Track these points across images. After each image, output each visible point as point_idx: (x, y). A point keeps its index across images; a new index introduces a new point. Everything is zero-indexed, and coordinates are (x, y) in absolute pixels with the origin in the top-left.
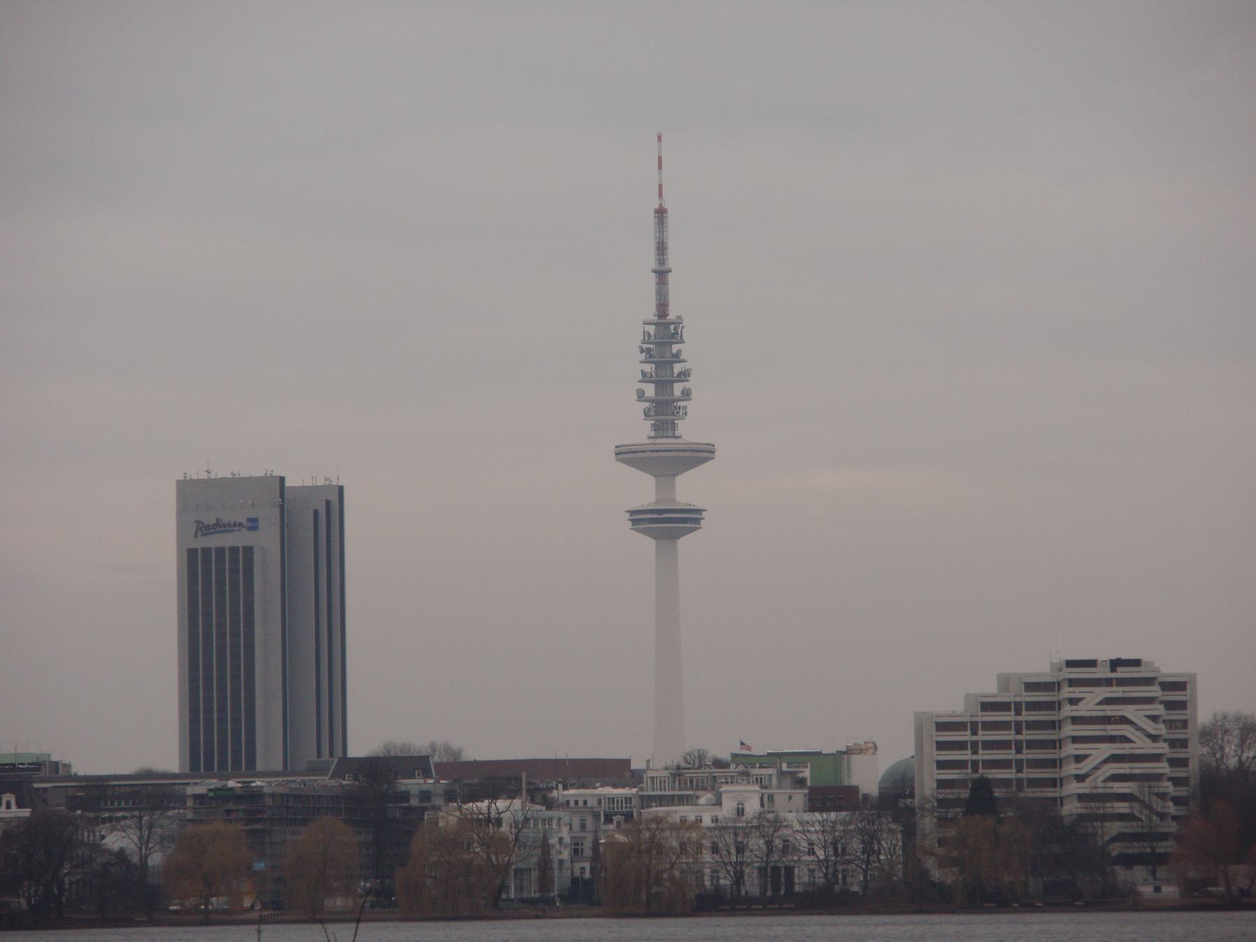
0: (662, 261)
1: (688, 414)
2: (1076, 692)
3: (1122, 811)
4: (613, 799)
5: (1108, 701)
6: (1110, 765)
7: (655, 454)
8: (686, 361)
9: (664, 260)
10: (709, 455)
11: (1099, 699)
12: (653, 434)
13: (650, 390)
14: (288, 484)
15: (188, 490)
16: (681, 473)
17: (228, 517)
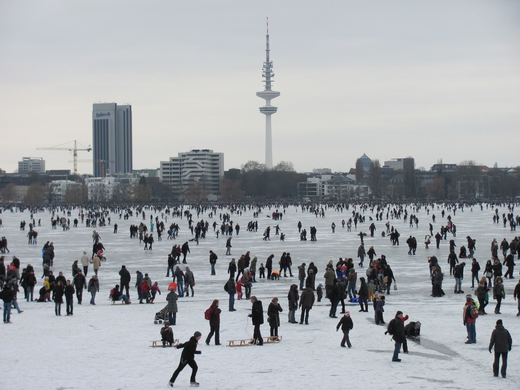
0: (268, 48)
2: (188, 157)
3: (186, 183)
5: (194, 159)
6: (191, 173)
7: (266, 94)
12: (265, 89)
14: (117, 105)
15: (95, 106)
16: (272, 99)
17: (103, 112)
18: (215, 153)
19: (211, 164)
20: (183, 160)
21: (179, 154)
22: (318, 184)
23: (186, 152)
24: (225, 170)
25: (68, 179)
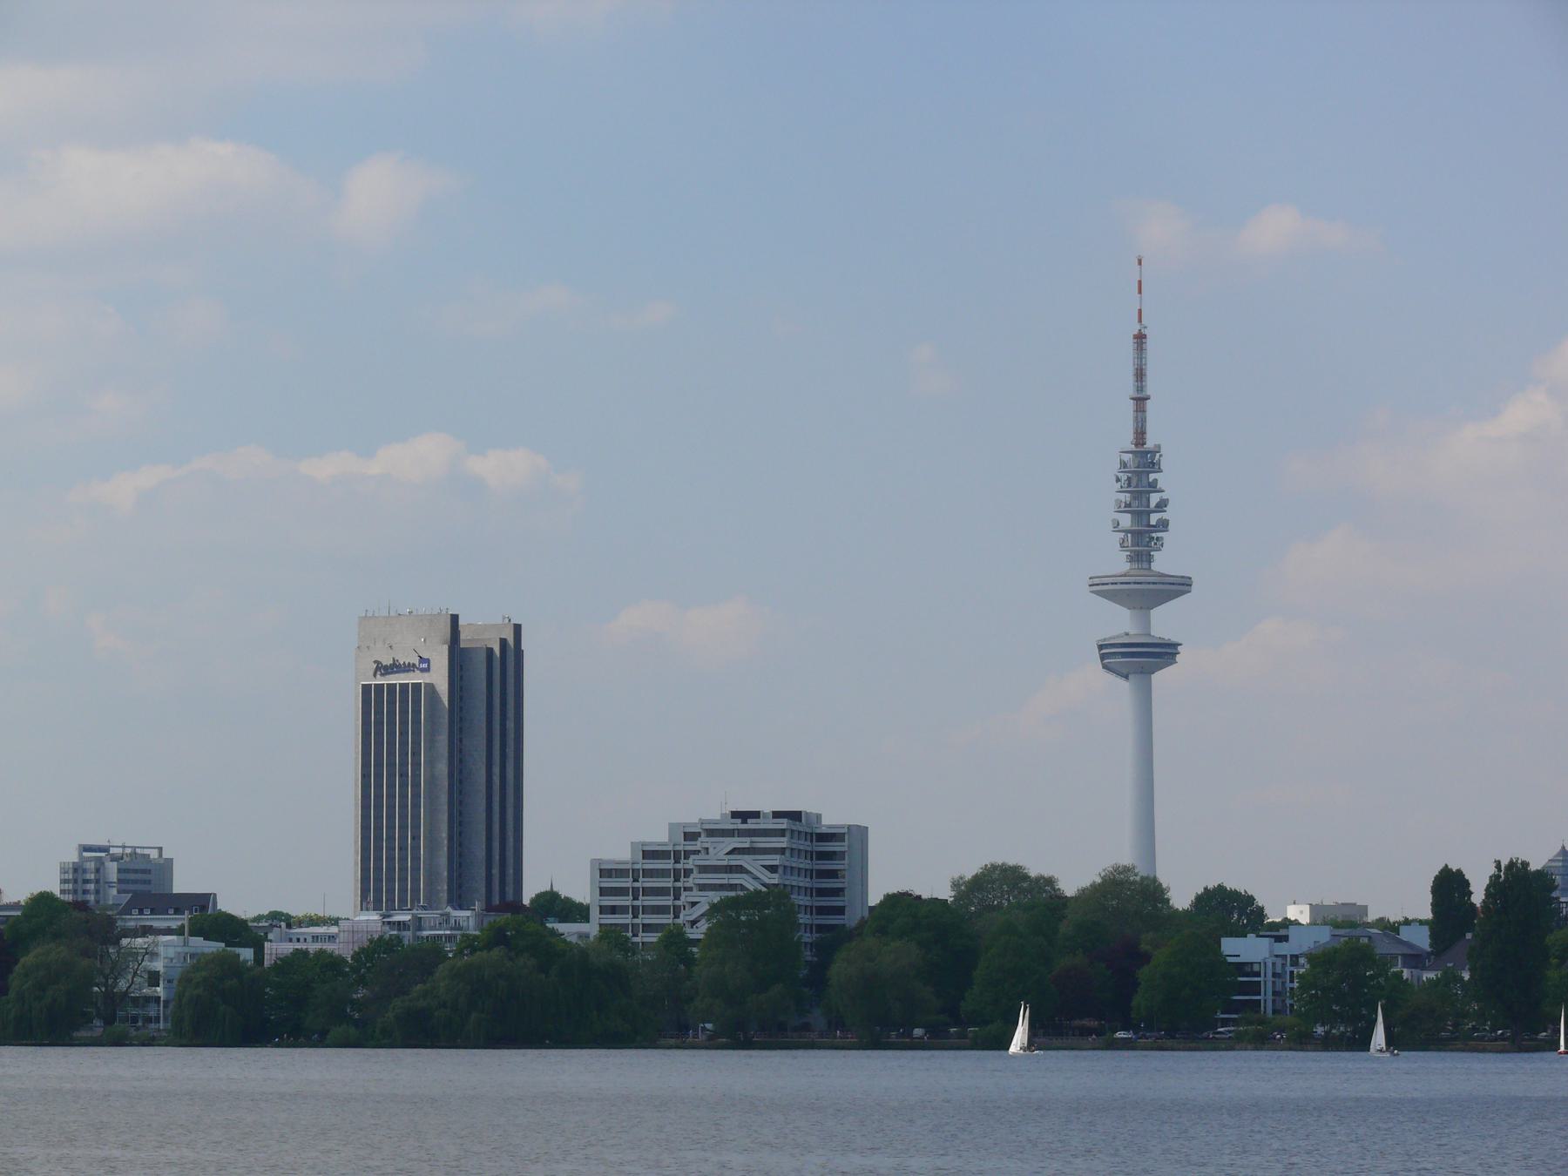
0: (1140, 388)
1: (1164, 545)
4: (317, 937)
5: (733, 851)
7: (1152, 586)
8: (1163, 491)
9: (1142, 387)
10: (1186, 588)
11: (729, 848)
13: (1126, 520)
17: (403, 659)
18: (830, 827)
19: (810, 873)
20: (687, 854)
21: (672, 827)
22: (1270, 965)
23: (702, 822)
24: (870, 905)
25: (192, 934)
